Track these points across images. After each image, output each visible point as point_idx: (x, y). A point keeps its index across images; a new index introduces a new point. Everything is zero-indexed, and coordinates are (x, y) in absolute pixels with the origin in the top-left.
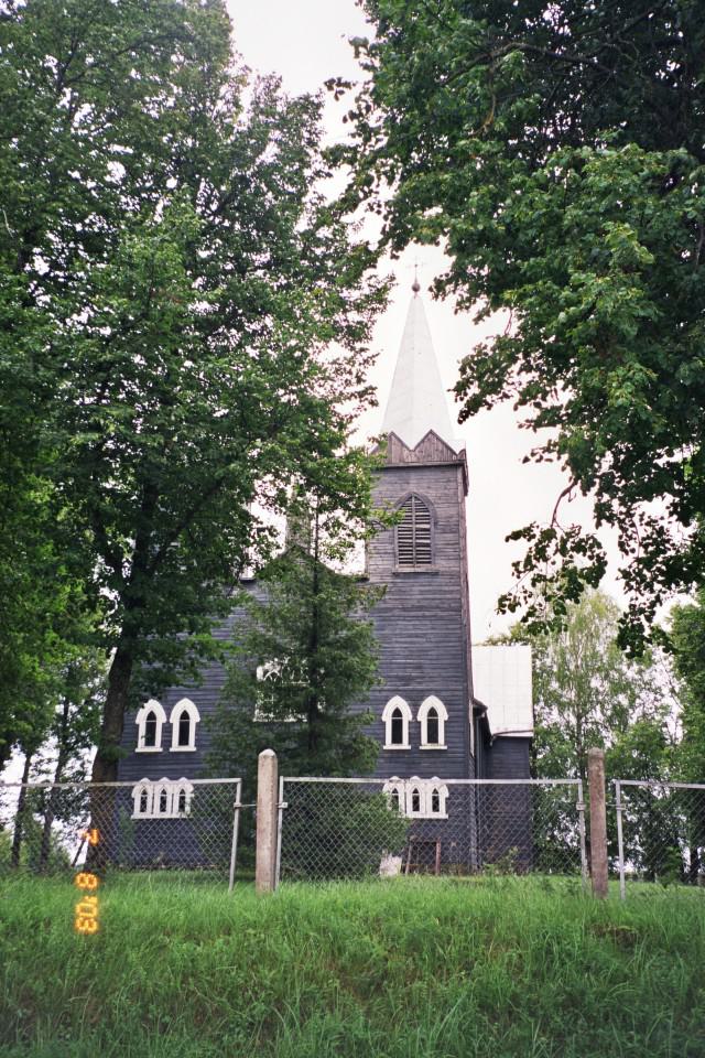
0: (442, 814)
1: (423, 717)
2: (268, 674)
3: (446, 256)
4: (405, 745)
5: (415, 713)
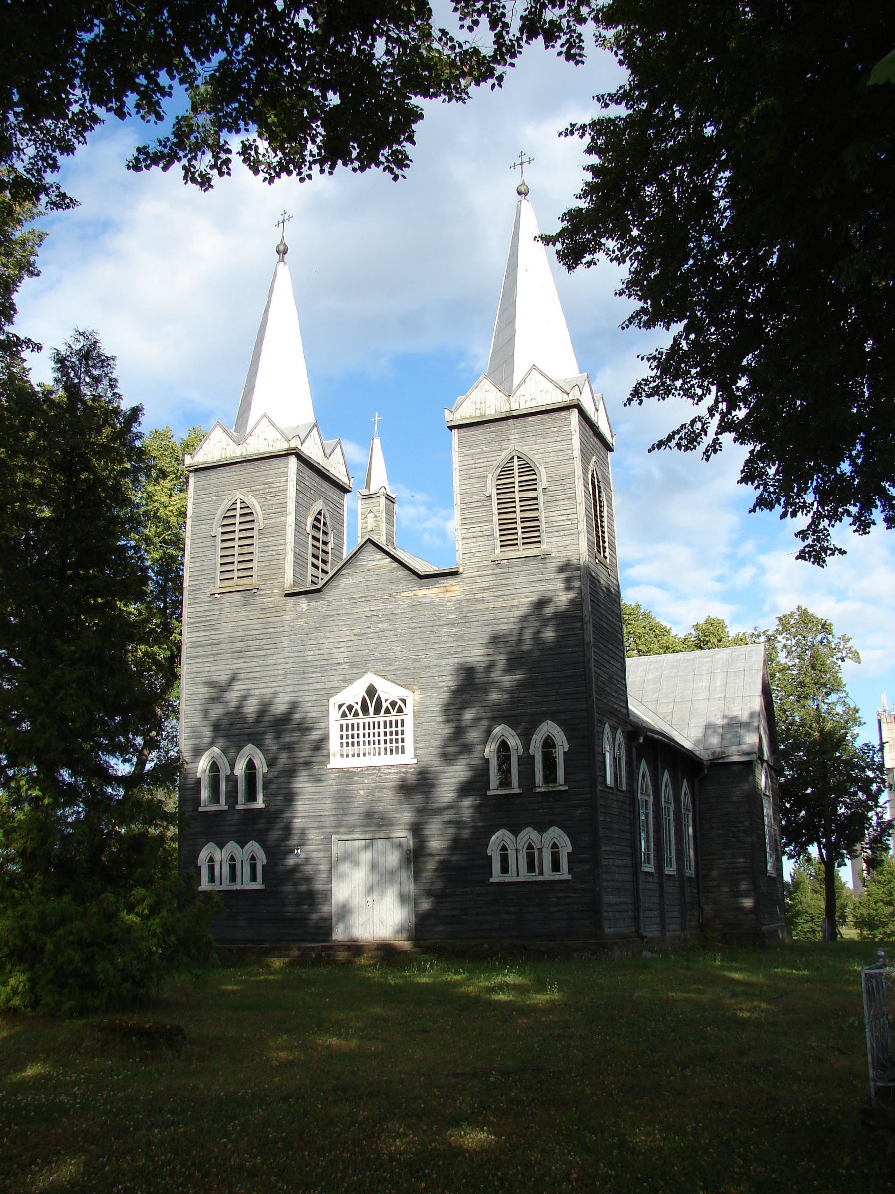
0: (564, 874)
1: (536, 748)
3: (75, 152)
4: (223, 806)
5: (526, 745)
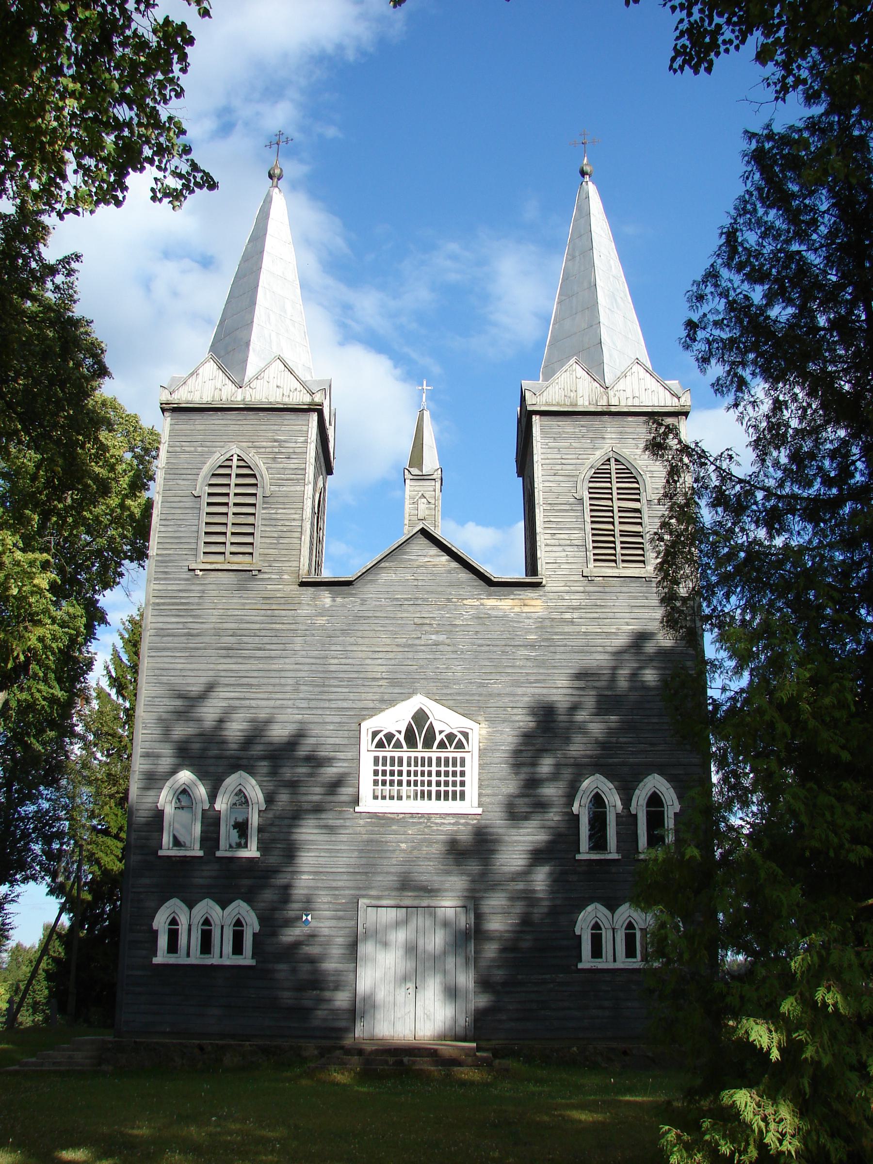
2: (381, 735)
